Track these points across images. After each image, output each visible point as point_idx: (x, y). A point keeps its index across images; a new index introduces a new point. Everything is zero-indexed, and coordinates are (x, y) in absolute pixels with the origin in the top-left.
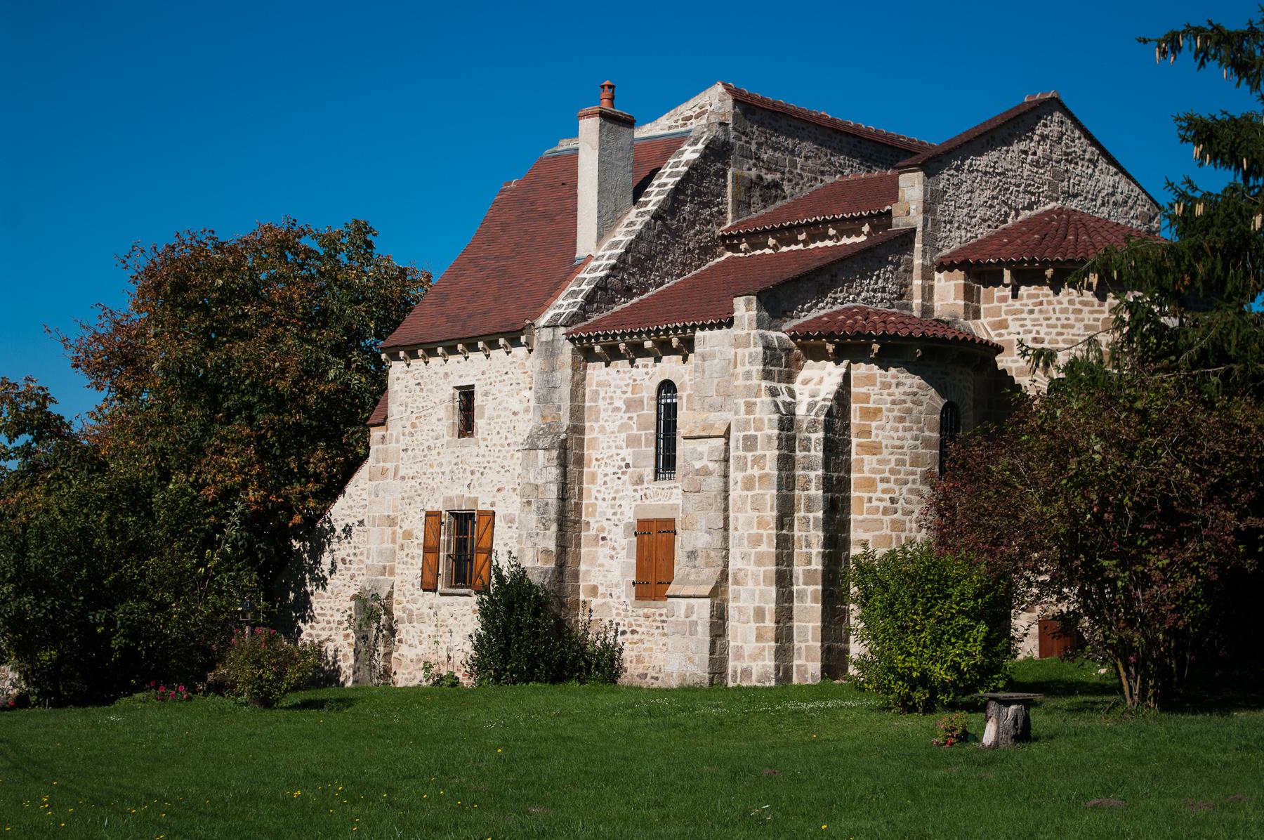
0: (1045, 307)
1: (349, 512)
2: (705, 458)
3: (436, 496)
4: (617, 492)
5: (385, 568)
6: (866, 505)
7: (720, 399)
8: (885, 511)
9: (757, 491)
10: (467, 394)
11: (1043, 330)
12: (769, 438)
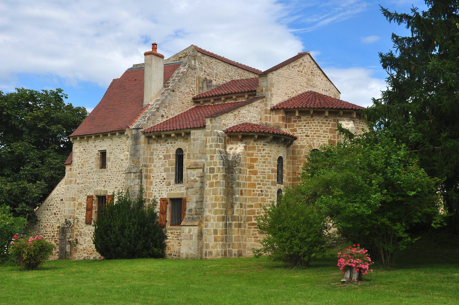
0: (310, 124)
1: (57, 196)
2: (195, 176)
3: (91, 190)
4: (160, 188)
5: (71, 216)
6: (252, 193)
7: (200, 155)
8: (259, 195)
9: (214, 188)
10: (103, 154)
11: (309, 132)
12: (219, 168)
